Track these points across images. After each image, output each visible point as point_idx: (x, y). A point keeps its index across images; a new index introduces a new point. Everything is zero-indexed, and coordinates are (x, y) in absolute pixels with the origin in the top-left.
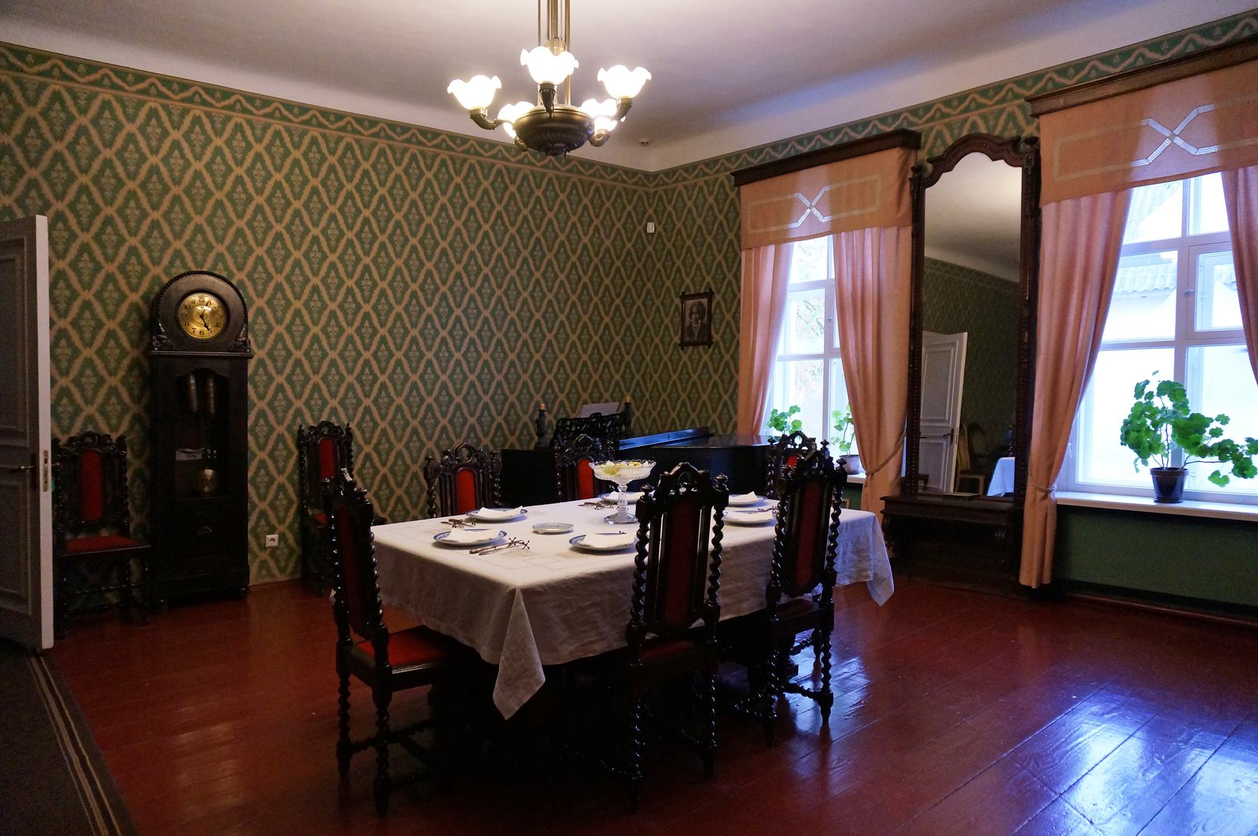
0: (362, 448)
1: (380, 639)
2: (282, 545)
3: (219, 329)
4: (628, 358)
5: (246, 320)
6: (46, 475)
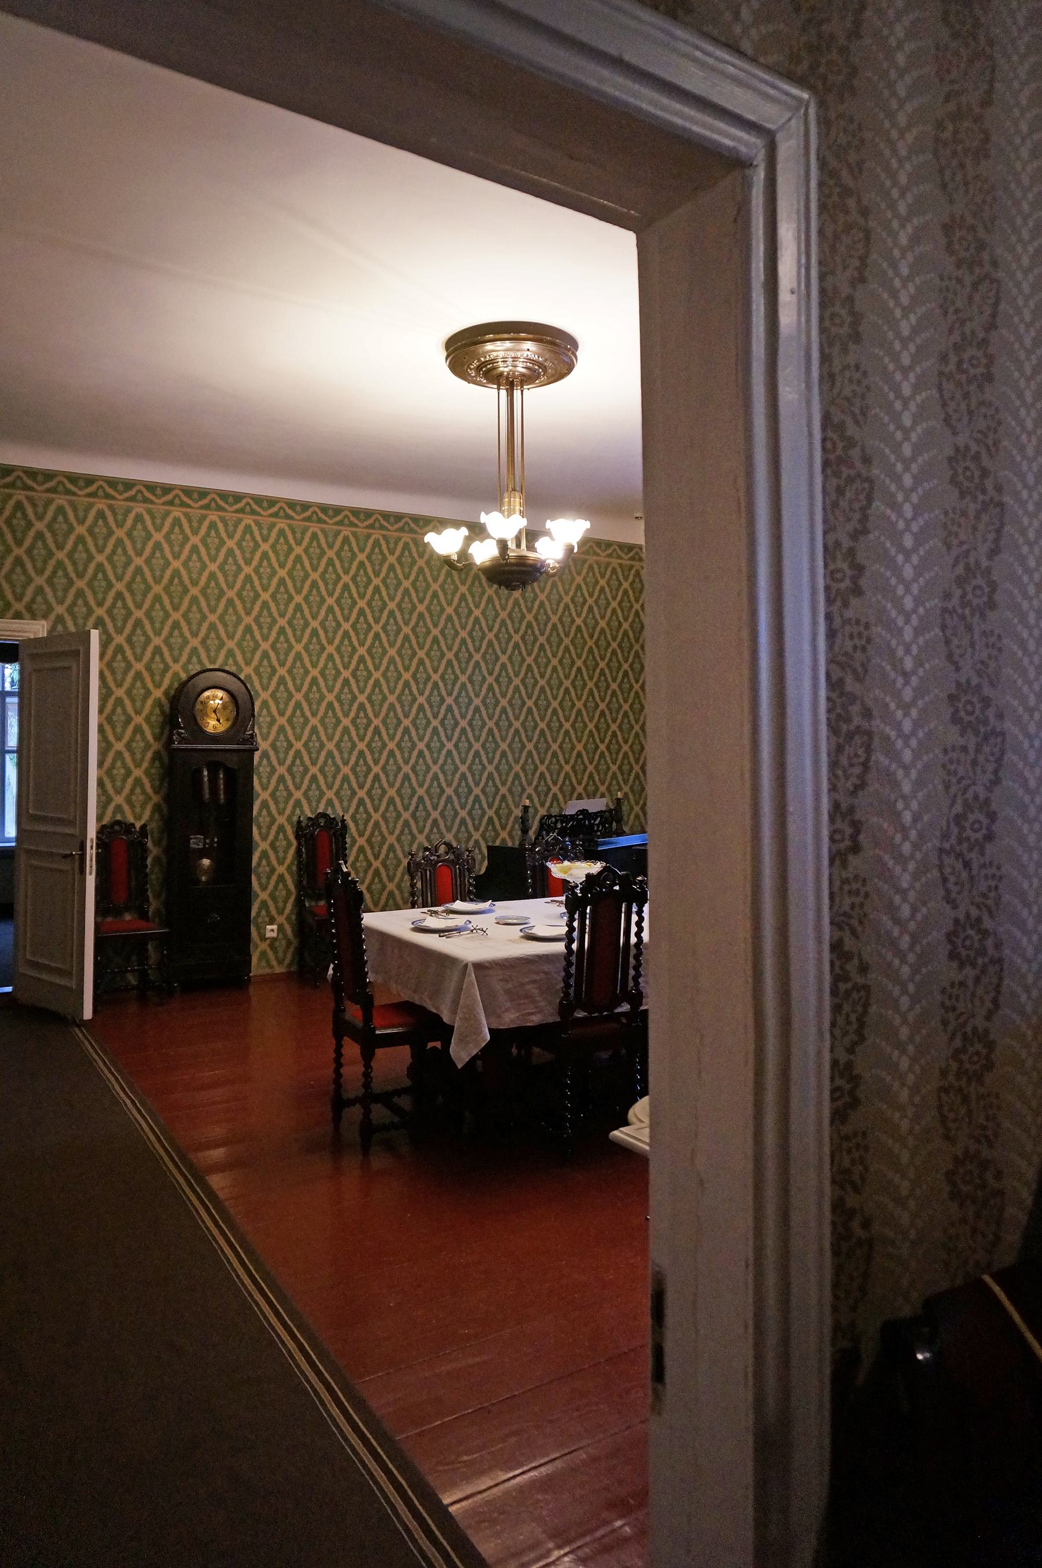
0: (356, 841)
1: (367, 1003)
2: (281, 936)
3: (230, 723)
4: (626, 748)
5: (253, 715)
6: (91, 860)
